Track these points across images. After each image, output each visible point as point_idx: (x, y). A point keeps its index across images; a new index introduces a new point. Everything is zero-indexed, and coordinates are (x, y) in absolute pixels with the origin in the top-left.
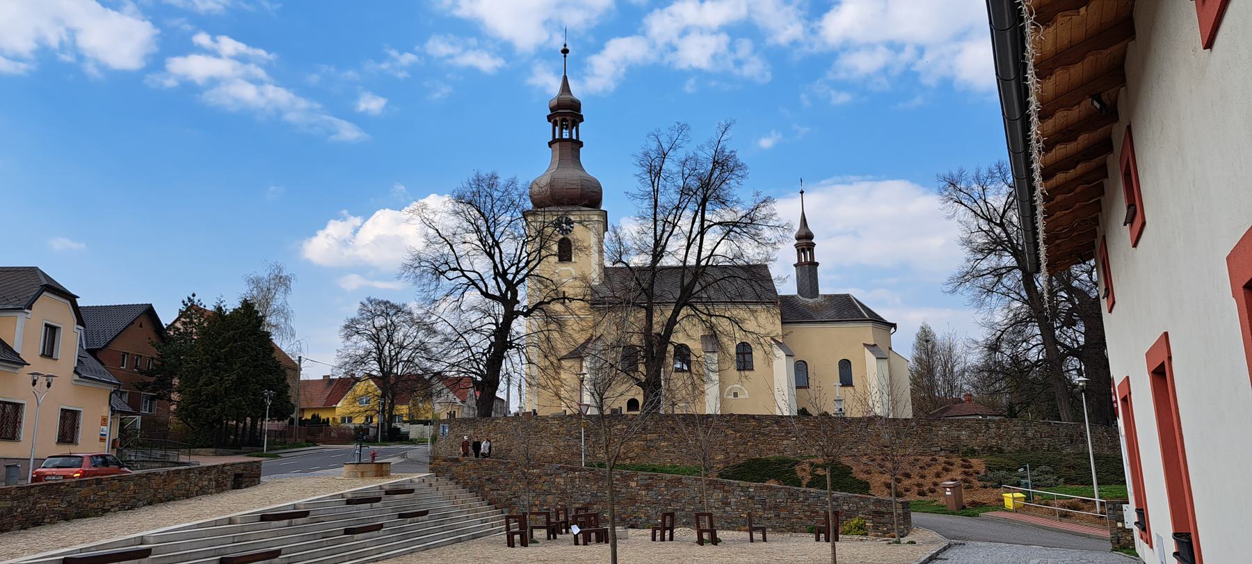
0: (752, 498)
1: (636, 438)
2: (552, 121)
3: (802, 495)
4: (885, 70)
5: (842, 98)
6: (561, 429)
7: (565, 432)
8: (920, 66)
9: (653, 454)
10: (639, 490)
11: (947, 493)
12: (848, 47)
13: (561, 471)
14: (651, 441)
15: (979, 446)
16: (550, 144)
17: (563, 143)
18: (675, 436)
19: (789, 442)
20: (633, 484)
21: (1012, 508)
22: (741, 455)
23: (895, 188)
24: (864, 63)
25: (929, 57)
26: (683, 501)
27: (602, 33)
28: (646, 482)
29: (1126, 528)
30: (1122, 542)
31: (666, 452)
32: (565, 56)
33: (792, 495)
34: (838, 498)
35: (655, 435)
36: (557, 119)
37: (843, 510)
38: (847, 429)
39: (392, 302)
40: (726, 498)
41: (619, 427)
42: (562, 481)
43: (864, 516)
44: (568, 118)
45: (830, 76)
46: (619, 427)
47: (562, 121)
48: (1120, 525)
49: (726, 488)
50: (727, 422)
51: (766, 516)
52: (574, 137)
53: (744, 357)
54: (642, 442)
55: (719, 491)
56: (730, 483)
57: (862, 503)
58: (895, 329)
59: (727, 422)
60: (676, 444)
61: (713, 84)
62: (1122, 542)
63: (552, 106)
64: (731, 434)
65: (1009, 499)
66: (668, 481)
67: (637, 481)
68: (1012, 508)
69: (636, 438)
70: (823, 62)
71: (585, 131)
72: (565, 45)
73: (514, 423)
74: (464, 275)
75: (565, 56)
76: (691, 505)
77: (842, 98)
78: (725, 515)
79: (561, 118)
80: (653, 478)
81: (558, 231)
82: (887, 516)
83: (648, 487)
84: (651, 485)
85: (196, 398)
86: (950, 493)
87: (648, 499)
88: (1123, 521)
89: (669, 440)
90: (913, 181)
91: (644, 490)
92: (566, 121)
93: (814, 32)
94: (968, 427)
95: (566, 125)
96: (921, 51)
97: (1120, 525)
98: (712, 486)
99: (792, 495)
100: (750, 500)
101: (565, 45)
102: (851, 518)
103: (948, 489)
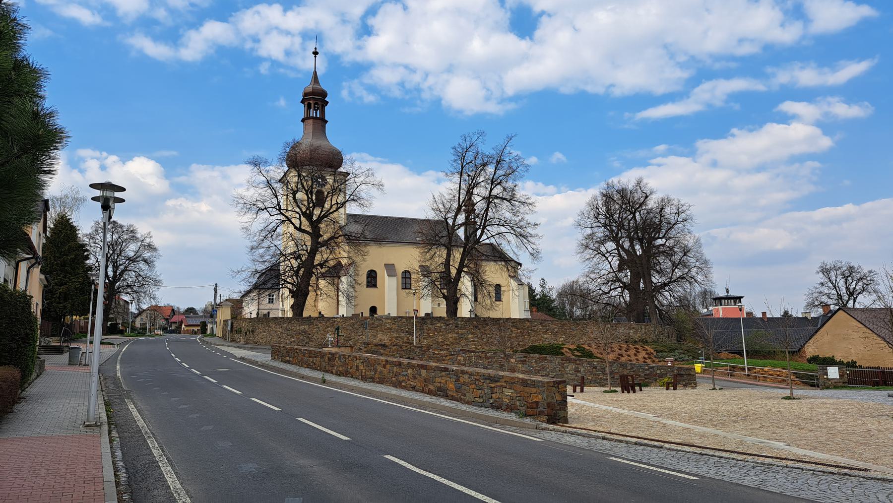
0: (595, 368)
1: (450, 332)
2: (306, 103)
3: (629, 366)
4: (402, 84)
5: (370, 98)
6: (394, 326)
7: (397, 328)
8: (425, 85)
9: (463, 343)
10: (517, 364)
11: (668, 364)
12: (382, 64)
13: (461, 352)
14: (462, 334)
15: (638, 339)
16: (303, 121)
17: (315, 121)
18: (478, 331)
19: (548, 335)
20: (513, 361)
21: (700, 372)
22: (520, 343)
23: (828, 208)
24: (386, 77)
25: (431, 80)
26: (548, 370)
27: (199, 18)
28: (522, 359)
29: (829, 378)
30: (827, 385)
31: (472, 341)
32: (315, 57)
33: (623, 365)
34: (653, 367)
35: (464, 330)
36: (311, 102)
37: (657, 374)
38: (577, 328)
39: (119, 223)
40: (578, 368)
41: (439, 325)
42: (462, 359)
43: (670, 376)
44: (319, 103)
45: (366, 80)
46: (439, 325)
47: (315, 104)
48: (825, 377)
49: (578, 362)
50: (512, 323)
51: (605, 378)
52: (314, 116)
53: (406, 280)
54: (455, 335)
55: (572, 364)
56: (580, 359)
57: (669, 369)
58: (521, 266)
59: (512, 323)
60: (479, 336)
61: (282, 70)
62: (827, 385)
63: (306, 92)
64: (515, 330)
65: (698, 367)
66: (538, 358)
67: (515, 359)
68: (700, 372)
69: (450, 332)
70: (361, 69)
71: (329, 112)
72: (316, 49)
73: (351, 321)
74: (281, 214)
75: (315, 57)
76: (553, 372)
77: (370, 98)
78: (577, 378)
79: (314, 102)
80: (526, 357)
81: (316, 185)
82: (685, 376)
83: (523, 362)
84: (525, 361)
85: (48, 296)
86: (670, 364)
87: (523, 369)
88: (827, 375)
89: (474, 334)
90: (404, 164)
91: (520, 364)
92: (318, 104)
93: (360, 48)
94: (633, 328)
95: (317, 107)
96: (427, 75)
97: (825, 377)
98: (568, 361)
99: (623, 365)
100: (594, 369)
101: (316, 49)
102: (662, 377)
103: (669, 362)
